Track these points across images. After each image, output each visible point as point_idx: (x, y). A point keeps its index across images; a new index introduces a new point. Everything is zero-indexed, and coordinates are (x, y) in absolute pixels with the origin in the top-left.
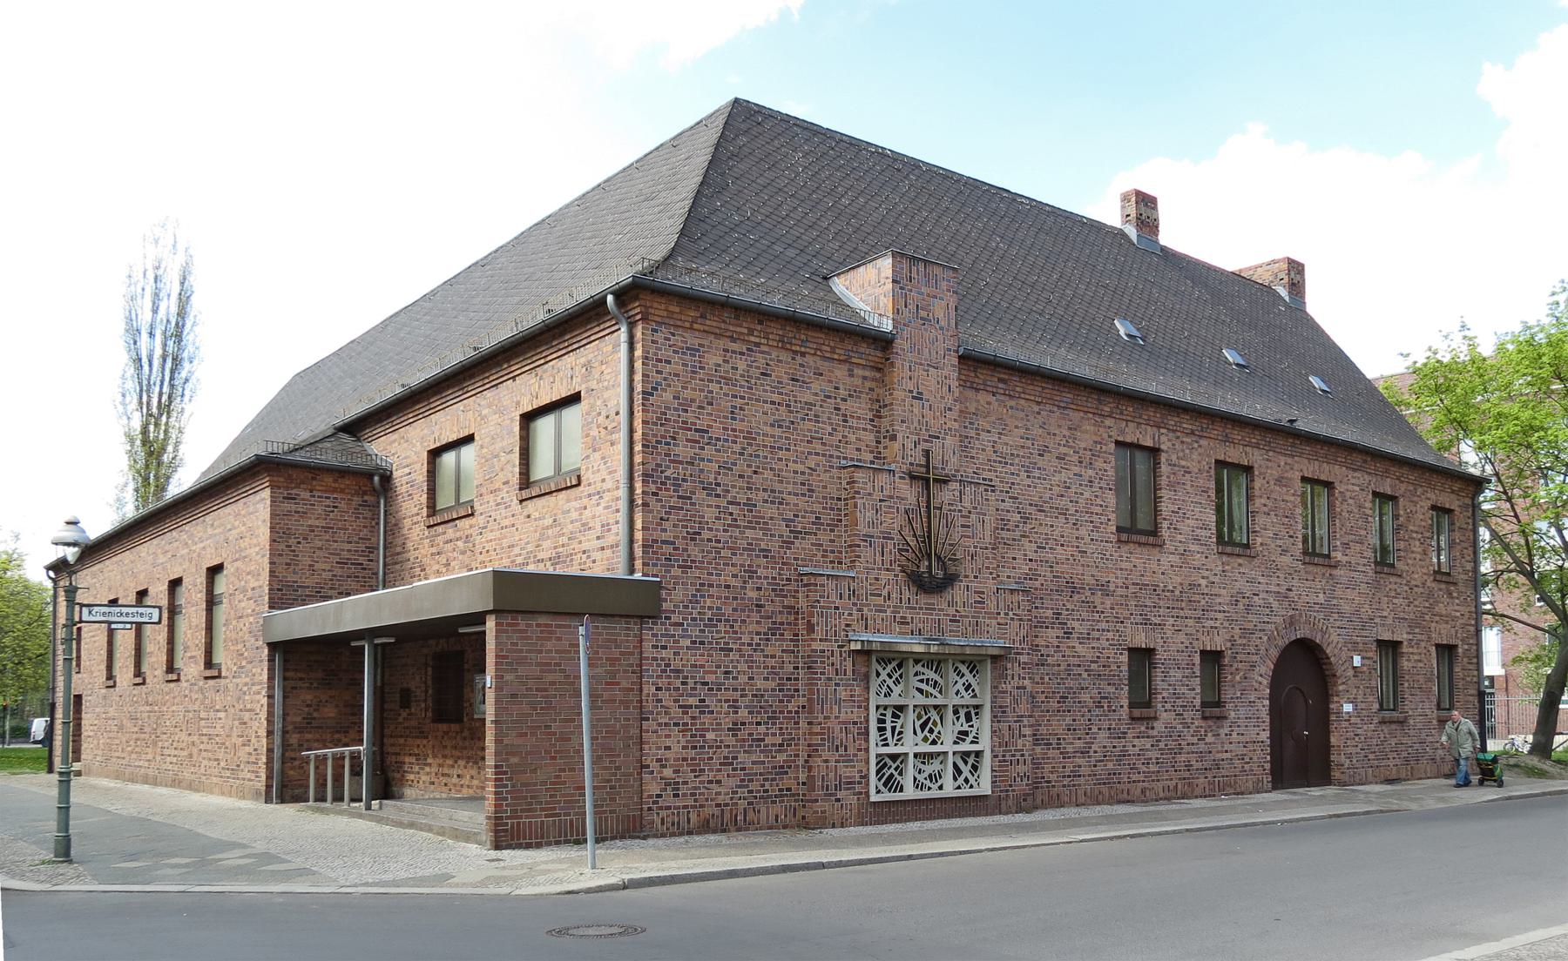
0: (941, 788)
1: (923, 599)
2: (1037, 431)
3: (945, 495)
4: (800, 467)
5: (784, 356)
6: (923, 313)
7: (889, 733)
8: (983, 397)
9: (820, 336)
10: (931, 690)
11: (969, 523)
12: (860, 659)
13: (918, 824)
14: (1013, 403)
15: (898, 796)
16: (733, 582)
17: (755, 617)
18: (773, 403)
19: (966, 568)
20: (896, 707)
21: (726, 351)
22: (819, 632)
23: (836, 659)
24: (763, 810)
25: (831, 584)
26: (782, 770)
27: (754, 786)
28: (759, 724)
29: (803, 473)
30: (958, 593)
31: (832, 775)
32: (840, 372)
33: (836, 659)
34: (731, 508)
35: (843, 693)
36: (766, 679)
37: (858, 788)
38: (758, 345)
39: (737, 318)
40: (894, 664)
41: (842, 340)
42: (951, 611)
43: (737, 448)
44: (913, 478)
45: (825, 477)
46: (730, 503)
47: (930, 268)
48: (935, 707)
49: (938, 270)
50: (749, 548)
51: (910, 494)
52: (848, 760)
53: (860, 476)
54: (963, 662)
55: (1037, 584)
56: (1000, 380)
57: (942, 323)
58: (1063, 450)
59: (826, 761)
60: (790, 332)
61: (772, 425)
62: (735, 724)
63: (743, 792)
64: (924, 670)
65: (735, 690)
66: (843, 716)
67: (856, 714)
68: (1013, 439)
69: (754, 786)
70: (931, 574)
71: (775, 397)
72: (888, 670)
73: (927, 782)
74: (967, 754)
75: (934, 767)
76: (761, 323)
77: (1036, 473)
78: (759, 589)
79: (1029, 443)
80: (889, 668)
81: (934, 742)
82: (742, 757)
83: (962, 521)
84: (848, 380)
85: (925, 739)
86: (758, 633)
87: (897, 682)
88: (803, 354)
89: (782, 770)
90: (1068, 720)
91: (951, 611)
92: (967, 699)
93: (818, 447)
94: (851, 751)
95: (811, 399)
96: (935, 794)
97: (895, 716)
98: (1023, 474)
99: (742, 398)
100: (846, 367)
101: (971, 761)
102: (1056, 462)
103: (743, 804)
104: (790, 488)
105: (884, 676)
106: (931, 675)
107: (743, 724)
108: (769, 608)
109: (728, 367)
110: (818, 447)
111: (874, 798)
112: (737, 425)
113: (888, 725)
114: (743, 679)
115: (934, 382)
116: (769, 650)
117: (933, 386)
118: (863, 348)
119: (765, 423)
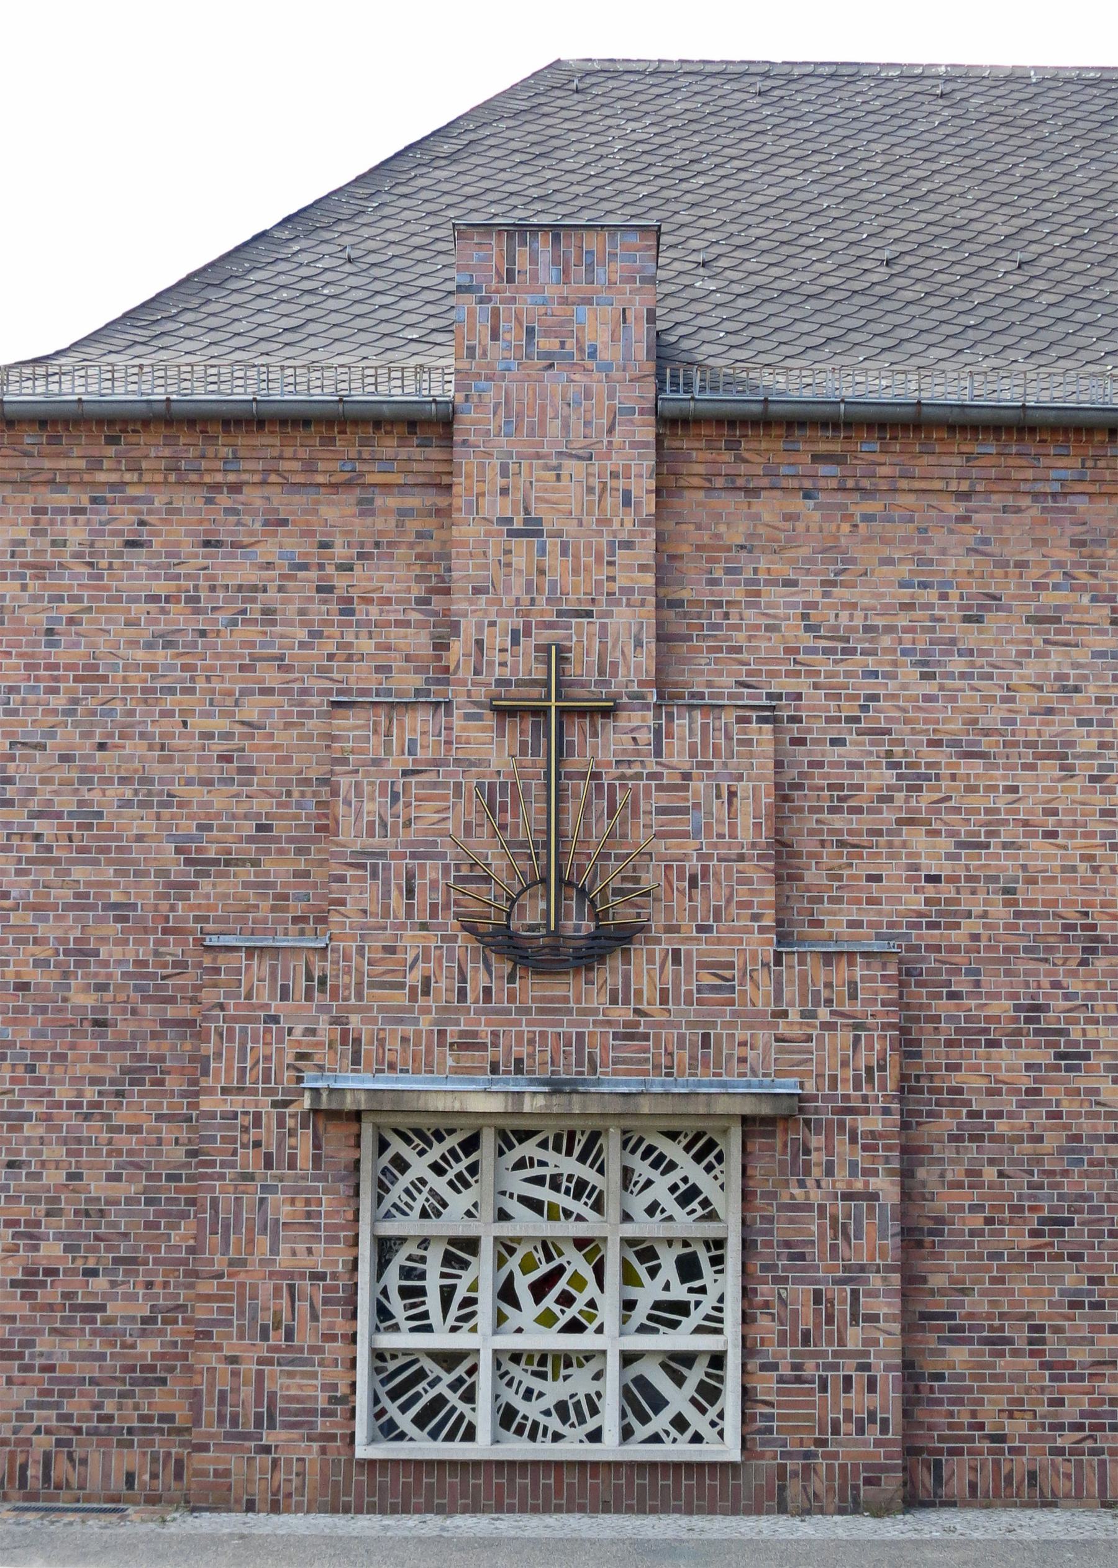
0: (595, 1436)
1: (533, 989)
2: (957, 562)
3: (604, 747)
4: (219, 724)
5: (185, 499)
6: (546, 344)
7: (432, 1302)
8: (769, 509)
9: (268, 442)
10: (564, 1201)
11: (691, 805)
12: (335, 1135)
13: (684, 1521)
14: (873, 506)
15: (458, 1450)
16: (36, 976)
17: (90, 1045)
18: (153, 599)
19: (677, 909)
20: (454, 1241)
21: (39, 511)
22: (221, 1074)
23: (269, 1134)
24: (95, 1459)
25: (260, 968)
26: (150, 1376)
27: (76, 1406)
28: (92, 1273)
29: (227, 736)
30: (644, 969)
31: (248, 1392)
32: (336, 512)
33: (269, 1134)
34: (38, 826)
35: (283, 1209)
36: (111, 1177)
37: (322, 1425)
38: (114, 486)
39: (54, 440)
40: (452, 1141)
41: (211, 439)
42: (622, 1013)
43: (59, 702)
44: (504, 713)
45: (286, 738)
46: (39, 815)
47: (570, 246)
48: (580, 1243)
49: (592, 242)
50: (81, 903)
51: (495, 751)
52: (294, 1359)
53: (348, 724)
54: (673, 1135)
55: (957, 937)
56: (817, 458)
57: (605, 355)
58: (1050, 599)
59: (233, 1360)
60: (188, 446)
61: (149, 646)
62: (30, 1272)
63: (46, 1417)
64: (549, 1155)
65: (33, 1200)
66: (283, 1261)
67: (326, 1257)
68: (878, 589)
69: (76, 1406)
70: (561, 929)
71: (161, 587)
72: (436, 1152)
73: (554, 1423)
74: (688, 1359)
75: (579, 1383)
76: (112, 440)
77: (957, 665)
78: (102, 988)
79: (931, 596)
80: (436, 1152)
81: (574, 1327)
82: (44, 1343)
83: (660, 799)
84: (358, 525)
85: (547, 1319)
86: (94, 1081)
87: (460, 1183)
88: (235, 488)
89: (150, 1376)
90: (1072, 1279)
91: (622, 1013)
92: (685, 1223)
93: (271, 676)
94: (305, 1338)
95: (253, 577)
96: (573, 1447)
97: (449, 1259)
98: (909, 673)
99: (73, 599)
100: (350, 497)
101: (696, 1375)
102: (1021, 631)
103: (43, 1443)
104: (191, 770)
105: (419, 1167)
106: (569, 1166)
107: (51, 1272)
108: (126, 1026)
109: (42, 543)
110: (271, 676)
111: (363, 1451)
112: (61, 655)
113: (433, 1284)
114: (54, 1177)
115: (574, 490)
116: (122, 1117)
117: (572, 493)
118: (388, 446)
119: (133, 644)
